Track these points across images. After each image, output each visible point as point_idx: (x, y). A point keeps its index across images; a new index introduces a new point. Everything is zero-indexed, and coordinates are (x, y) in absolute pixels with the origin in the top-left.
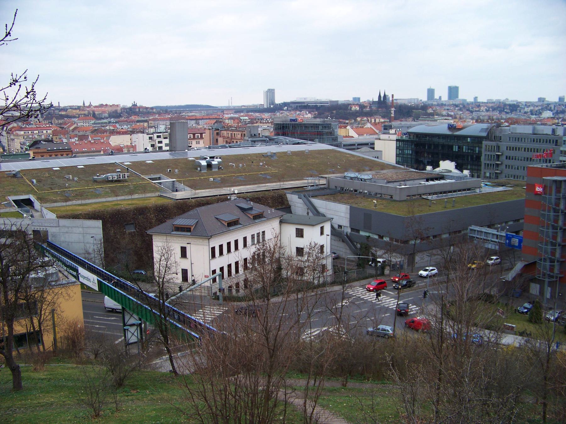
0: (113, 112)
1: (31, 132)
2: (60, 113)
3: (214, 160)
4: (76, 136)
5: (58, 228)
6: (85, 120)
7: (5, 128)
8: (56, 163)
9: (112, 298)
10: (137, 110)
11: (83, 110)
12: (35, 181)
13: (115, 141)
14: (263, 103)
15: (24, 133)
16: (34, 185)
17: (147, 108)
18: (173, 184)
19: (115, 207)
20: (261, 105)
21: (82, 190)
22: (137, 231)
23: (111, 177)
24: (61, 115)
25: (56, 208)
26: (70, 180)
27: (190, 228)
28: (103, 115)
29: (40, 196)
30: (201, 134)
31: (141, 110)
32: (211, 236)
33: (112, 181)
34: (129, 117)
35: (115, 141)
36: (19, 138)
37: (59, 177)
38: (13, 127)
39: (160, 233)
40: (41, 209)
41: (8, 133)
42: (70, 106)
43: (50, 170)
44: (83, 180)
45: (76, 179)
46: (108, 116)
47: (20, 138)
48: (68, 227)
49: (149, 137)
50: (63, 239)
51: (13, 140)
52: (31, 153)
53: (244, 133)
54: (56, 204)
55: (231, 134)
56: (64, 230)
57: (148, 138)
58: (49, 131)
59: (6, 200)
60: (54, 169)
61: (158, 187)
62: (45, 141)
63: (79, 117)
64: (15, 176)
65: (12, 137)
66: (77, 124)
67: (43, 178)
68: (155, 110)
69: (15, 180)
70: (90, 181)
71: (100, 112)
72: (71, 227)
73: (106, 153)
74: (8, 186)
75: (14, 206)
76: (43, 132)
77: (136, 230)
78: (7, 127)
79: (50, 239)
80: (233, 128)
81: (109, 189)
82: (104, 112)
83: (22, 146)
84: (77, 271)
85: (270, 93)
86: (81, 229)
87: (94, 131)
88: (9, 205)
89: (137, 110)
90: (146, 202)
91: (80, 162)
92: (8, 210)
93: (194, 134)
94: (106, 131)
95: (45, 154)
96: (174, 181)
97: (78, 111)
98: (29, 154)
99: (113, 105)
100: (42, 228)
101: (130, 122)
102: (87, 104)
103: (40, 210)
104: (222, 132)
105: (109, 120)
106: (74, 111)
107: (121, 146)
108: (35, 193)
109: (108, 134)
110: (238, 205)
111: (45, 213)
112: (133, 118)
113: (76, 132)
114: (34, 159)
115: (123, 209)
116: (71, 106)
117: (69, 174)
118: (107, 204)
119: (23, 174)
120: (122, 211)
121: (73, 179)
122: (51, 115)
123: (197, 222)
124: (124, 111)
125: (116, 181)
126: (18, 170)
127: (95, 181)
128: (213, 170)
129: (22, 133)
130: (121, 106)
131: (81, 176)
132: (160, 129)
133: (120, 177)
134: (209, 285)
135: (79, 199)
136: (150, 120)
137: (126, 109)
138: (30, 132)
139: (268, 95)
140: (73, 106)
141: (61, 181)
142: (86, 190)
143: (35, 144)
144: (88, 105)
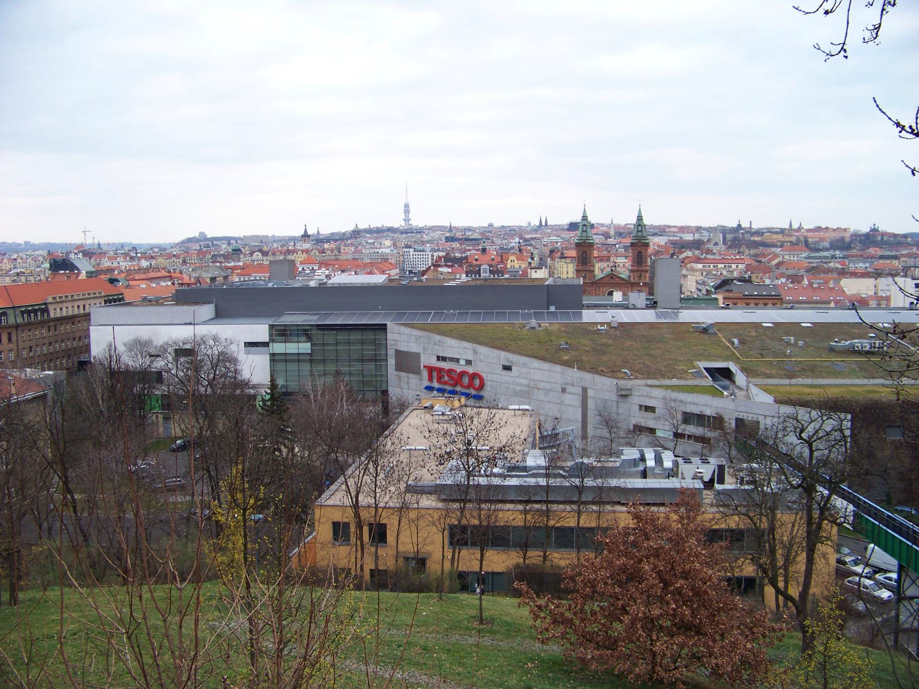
0: (838, 240)
1: (714, 266)
2: (752, 238)
4: (782, 275)
6: (794, 250)
8: (768, 316)
9: (886, 550)
10: (879, 238)
11: (789, 235)
12: (736, 341)
13: (852, 287)
15: (704, 266)
17: (895, 236)
19: (870, 396)
21: (813, 363)
23: (859, 345)
24: (754, 242)
25: (772, 388)
26: (791, 344)
28: (822, 244)
29: (745, 366)
31: (885, 239)
33: (859, 353)
34: (864, 250)
35: (852, 287)
36: (695, 274)
37: (773, 339)
38: (687, 257)
40: (748, 386)
42: (767, 229)
43: (757, 326)
44: (812, 346)
45: (800, 343)
46: (829, 246)
47: (697, 274)
51: (685, 276)
52: (720, 297)
54: (770, 381)
57: (914, 286)
58: (740, 266)
59: (694, 367)
60: (765, 325)
62: (739, 280)
63: (782, 246)
64: (705, 331)
65: (684, 272)
66: (783, 257)
67: (747, 338)
68: (909, 240)
69: (706, 336)
71: (817, 240)
73: (839, 306)
74: (696, 345)
75: (706, 377)
76: (731, 267)
77: (904, 437)
81: (856, 364)
82: (822, 240)
83: (700, 287)
87: (811, 270)
88: (698, 374)
89: (879, 238)
91: (806, 317)
92: (697, 382)
94: (830, 271)
95: (739, 301)
97: (780, 237)
98: (716, 299)
99: (838, 229)
100: (751, 415)
101: (867, 258)
102: (795, 226)
103: (745, 388)
105: (832, 252)
106: (775, 236)
107: (863, 296)
108: (737, 361)
109: (835, 275)
111: (754, 393)
112: (872, 251)
113: (782, 270)
114: (727, 307)
115: (884, 400)
116: (769, 228)
117: (788, 335)
118: (854, 389)
119: (717, 328)
121: (796, 344)
122: (738, 241)
125: (867, 353)
126: (710, 322)
127: (832, 350)
129: (700, 266)
130: (852, 230)
131: (807, 340)
135: (807, 377)
136: (902, 255)
137: (860, 235)
138: (712, 266)
140: (773, 228)
141: (776, 345)
142: (818, 363)
143: (724, 284)
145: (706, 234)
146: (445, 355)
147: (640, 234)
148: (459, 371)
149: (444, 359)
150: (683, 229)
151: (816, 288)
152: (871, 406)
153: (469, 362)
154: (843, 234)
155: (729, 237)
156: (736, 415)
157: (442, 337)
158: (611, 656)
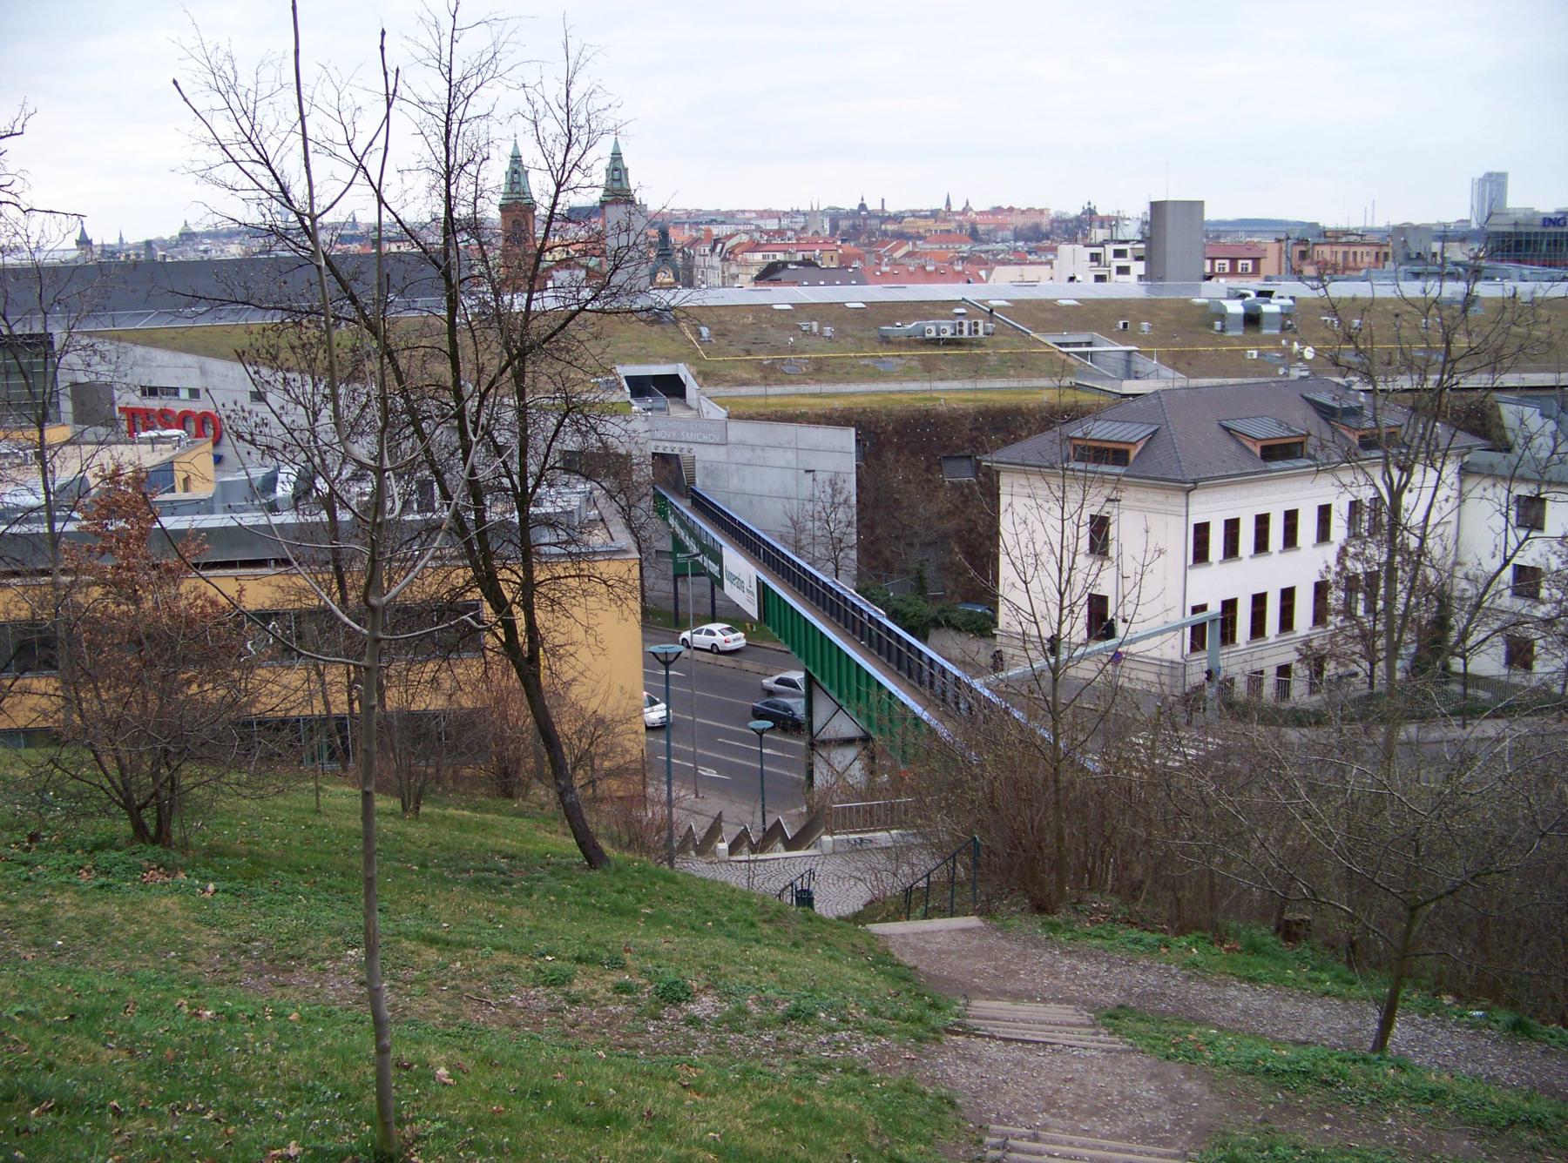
3: (1269, 302)
5: (722, 449)
6: (947, 242)
7: (719, 246)
11: (945, 220)
14: (1467, 217)
15: (764, 257)
16: (701, 343)
18: (1129, 362)
20: (1462, 221)
22: (980, 483)
23: (933, 328)
25: (740, 400)
27: (1126, 452)
28: (1000, 234)
30: (1256, 260)
32: (1195, 482)
33: (936, 342)
37: (781, 327)
38: (739, 244)
39: (1024, 467)
41: (724, 259)
42: (911, 211)
43: (766, 308)
45: (828, 331)
48: (753, 447)
49: (1092, 255)
50: (734, 483)
53: (1386, 249)
55: (1345, 253)
56: (743, 455)
57: (1088, 258)
60: (776, 307)
61: (1075, 363)
65: (734, 270)
70: (870, 339)
71: (992, 227)
72: (763, 448)
77: (976, 477)
78: (724, 244)
79: (699, 485)
80: (1352, 238)
82: (1002, 227)
84: (718, 559)
85: (1494, 183)
86: (790, 455)
90: (1024, 397)
91: (854, 296)
93: (1234, 261)
96: (1130, 352)
97: (931, 222)
99: (1029, 210)
100: (677, 445)
102: (957, 206)
104: (1318, 248)
106: (921, 222)
108: (690, 357)
110: (1311, 396)
120: (938, 415)
123: (1154, 433)
124: (1059, 228)
125: (949, 343)
127: (886, 340)
128: (1265, 332)
130: (1053, 213)
132: (1126, 230)
133: (961, 332)
134: (1178, 658)
137: (1065, 221)
139: (1484, 191)
144: (960, 209)
145: (801, 219)
146: (154, 384)
147: (617, 185)
148: (178, 411)
149: (152, 392)
150: (763, 214)
151: (931, 273)
152: (917, 421)
153: (194, 393)
154: (1037, 219)
155: (844, 224)
156: (651, 448)
157: (147, 349)
158: (851, 1038)
